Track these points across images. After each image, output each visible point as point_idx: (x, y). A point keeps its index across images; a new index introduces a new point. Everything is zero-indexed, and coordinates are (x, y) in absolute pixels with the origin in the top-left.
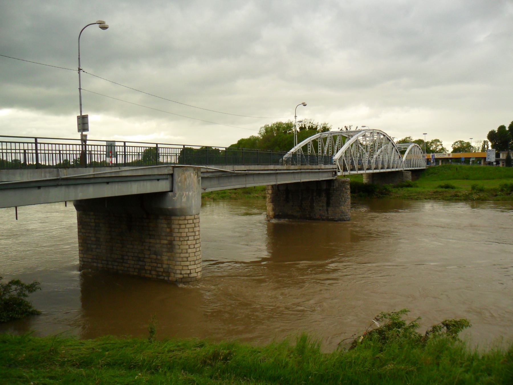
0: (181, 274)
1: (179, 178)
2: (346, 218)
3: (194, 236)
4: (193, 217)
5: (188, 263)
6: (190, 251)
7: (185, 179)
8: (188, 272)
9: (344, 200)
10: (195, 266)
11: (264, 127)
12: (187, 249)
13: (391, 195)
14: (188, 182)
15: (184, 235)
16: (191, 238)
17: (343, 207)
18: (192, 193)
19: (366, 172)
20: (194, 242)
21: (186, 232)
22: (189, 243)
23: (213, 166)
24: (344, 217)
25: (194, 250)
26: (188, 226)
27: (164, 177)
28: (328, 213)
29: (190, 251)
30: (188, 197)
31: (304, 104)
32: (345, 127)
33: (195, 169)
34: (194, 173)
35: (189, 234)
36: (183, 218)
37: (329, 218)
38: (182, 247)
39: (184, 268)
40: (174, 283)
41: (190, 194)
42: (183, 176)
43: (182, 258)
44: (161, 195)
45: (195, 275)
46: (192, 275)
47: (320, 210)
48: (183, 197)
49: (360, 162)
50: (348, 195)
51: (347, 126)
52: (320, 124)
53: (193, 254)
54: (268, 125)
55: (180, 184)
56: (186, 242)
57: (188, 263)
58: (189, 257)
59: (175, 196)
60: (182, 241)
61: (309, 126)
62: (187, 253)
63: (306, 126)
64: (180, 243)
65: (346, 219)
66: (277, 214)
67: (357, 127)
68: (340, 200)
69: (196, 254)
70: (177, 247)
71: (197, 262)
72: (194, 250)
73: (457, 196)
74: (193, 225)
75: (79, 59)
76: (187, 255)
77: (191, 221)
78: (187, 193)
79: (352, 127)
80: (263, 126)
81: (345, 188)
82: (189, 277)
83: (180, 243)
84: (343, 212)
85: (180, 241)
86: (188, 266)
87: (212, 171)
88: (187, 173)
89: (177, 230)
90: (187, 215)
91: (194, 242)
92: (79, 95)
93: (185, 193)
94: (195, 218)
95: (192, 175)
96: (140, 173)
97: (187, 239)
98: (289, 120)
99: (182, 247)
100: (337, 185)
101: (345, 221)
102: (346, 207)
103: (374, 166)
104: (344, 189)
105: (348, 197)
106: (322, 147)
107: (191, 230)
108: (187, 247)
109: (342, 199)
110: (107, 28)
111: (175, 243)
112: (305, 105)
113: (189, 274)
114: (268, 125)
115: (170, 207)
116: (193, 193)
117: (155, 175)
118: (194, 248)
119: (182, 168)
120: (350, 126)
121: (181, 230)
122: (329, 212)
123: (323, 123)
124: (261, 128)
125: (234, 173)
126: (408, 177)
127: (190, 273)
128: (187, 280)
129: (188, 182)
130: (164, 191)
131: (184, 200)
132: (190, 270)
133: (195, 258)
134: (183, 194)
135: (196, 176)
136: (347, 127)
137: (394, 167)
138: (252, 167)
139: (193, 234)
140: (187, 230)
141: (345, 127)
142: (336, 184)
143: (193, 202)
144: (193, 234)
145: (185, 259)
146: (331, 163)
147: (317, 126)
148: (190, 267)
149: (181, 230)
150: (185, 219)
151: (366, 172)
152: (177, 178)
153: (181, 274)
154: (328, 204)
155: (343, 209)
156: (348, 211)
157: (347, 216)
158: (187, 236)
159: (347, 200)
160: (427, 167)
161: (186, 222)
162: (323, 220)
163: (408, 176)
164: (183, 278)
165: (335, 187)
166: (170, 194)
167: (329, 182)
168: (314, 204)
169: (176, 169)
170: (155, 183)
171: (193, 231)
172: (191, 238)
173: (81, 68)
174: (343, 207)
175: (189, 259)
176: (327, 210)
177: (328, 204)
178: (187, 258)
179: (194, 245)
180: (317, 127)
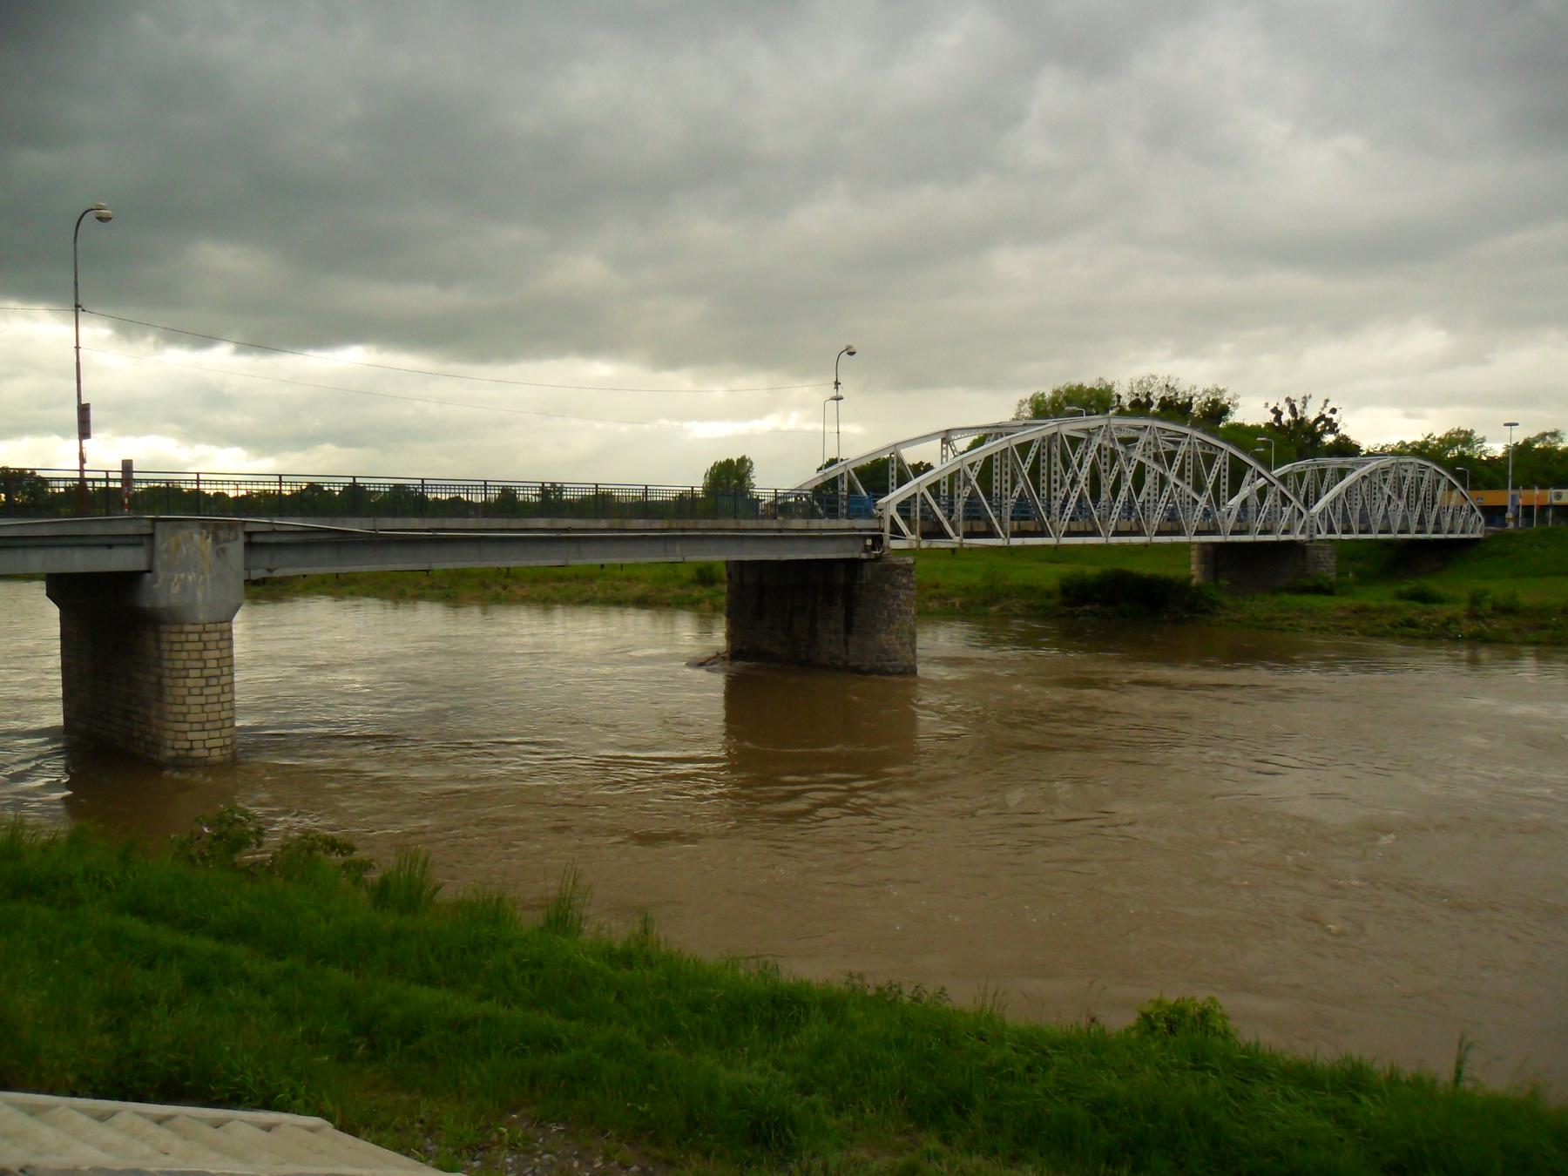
0: (173, 748)
1: (165, 544)
2: (891, 666)
3: (202, 669)
4: (200, 628)
5: (186, 727)
6: (190, 700)
7: (178, 546)
8: (187, 745)
9: (889, 615)
10: (204, 735)
11: (1031, 399)
12: (184, 696)
13: (1219, 614)
14: (185, 551)
15: (179, 664)
16: (192, 673)
17: (883, 636)
18: (194, 575)
19: (1058, 541)
20: (202, 682)
21: (184, 660)
22: (189, 682)
23: (328, 519)
24: (886, 663)
25: (202, 700)
26: (188, 646)
27: (131, 541)
28: (847, 651)
29: (190, 700)
30: (184, 585)
31: (851, 350)
32: (1288, 400)
33: (203, 525)
34: (201, 534)
35: (189, 664)
36: (176, 628)
37: (850, 664)
38: (177, 691)
39: (180, 736)
40: (160, 767)
41: (190, 578)
42: (173, 540)
43: (175, 714)
44: (131, 580)
45: (204, 753)
46: (195, 753)
47: (830, 641)
48: (173, 583)
49: (1364, 517)
50: (900, 602)
51: (1297, 397)
52: (1200, 391)
53: (199, 709)
54: (1043, 395)
55: (165, 557)
56: (182, 680)
57: (186, 727)
58: (189, 713)
59: (156, 582)
60: (176, 678)
61: (1163, 399)
62: (184, 704)
63: (1151, 397)
64: (171, 682)
65: (891, 670)
66: (737, 647)
67: (1327, 401)
68: (877, 615)
69: (207, 708)
70: (168, 691)
71: (208, 726)
72: (202, 700)
73: (1412, 626)
74: (201, 645)
75: (76, 284)
76: (184, 709)
77: (195, 637)
78: (183, 575)
79: (1311, 399)
80: (1028, 398)
81: (892, 585)
82: (188, 757)
83: (171, 682)
84: (884, 651)
85: (170, 677)
86: (186, 732)
87: (291, 529)
88: (182, 534)
89: (166, 655)
90: (185, 623)
91: (202, 682)
92: (75, 360)
93: (176, 575)
94: (207, 629)
95: (197, 537)
96: (45, 531)
97: (183, 673)
98: (1101, 379)
99: (177, 691)
100: (869, 575)
101: (890, 674)
102: (893, 637)
103: (1397, 525)
104: (887, 587)
105: (899, 610)
106: (1011, 471)
107: (195, 655)
108: (185, 692)
109: (881, 614)
110: (111, 219)
111: (166, 681)
112: (852, 354)
113: (187, 750)
114: (1043, 395)
115: (147, 605)
116: (198, 577)
117: (128, 535)
118: (201, 694)
119: (171, 523)
120: (1305, 398)
121: (174, 655)
122: (850, 648)
123: (1210, 386)
124: (1022, 403)
125: (377, 535)
126: (1321, 562)
127: (192, 749)
128: (184, 762)
129: (185, 551)
130: (140, 569)
131: (175, 589)
132: (192, 741)
133: (203, 717)
134: (172, 580)
135: (210, 540)
136: (1295, 401)
137: (1274, 530)
138: (592, 523)
139: (200, 664)
140: (184, 655)
141: (1288, 400)
142: (868, 571)
143: (199, 595)
144: (200, 664)
145: (181, 718)
146: (871, 516)
147: (1191, 398)
148: (191, 736)
149: (174, 655)
150: (181, 632)
151: (1058, 541)
152: (161, 544)
153: (173, 748)
154: (849, 627)
155: (884, 643)
156: (901, 647)
157: (896, 660)
158: (185, 669)
159: (898, 616)
160: (1489, 534)
161: (183, 637)
162: (838, 669)
163: (1322, 560)
164: (177, 757)
165: (864, 581)
166: (148, 576)
167: (853, 565)
168: (818, 626)
169: (158, 524)
170: (106, 552)
171: (198, 657)
172: (192, 673)
173: (79, 303)
174: (883, 636)
175: (190, 718)
176: (846, 643)
177: (849, 627)
178: (184, 714)
179: (202, 688)
180: (1193, 402)
